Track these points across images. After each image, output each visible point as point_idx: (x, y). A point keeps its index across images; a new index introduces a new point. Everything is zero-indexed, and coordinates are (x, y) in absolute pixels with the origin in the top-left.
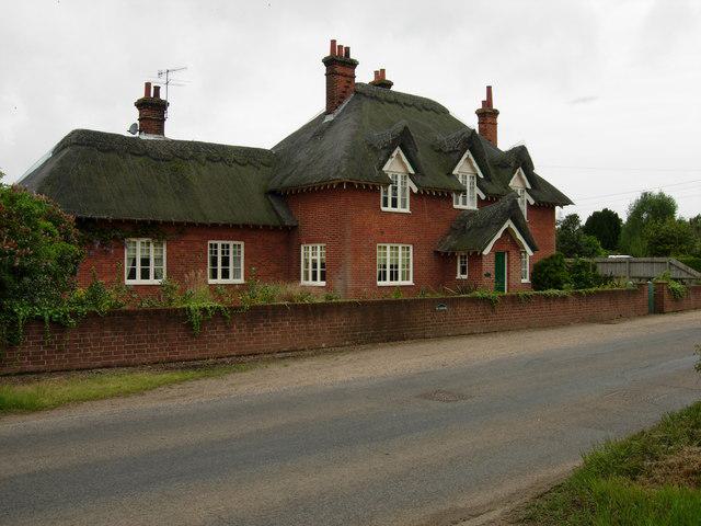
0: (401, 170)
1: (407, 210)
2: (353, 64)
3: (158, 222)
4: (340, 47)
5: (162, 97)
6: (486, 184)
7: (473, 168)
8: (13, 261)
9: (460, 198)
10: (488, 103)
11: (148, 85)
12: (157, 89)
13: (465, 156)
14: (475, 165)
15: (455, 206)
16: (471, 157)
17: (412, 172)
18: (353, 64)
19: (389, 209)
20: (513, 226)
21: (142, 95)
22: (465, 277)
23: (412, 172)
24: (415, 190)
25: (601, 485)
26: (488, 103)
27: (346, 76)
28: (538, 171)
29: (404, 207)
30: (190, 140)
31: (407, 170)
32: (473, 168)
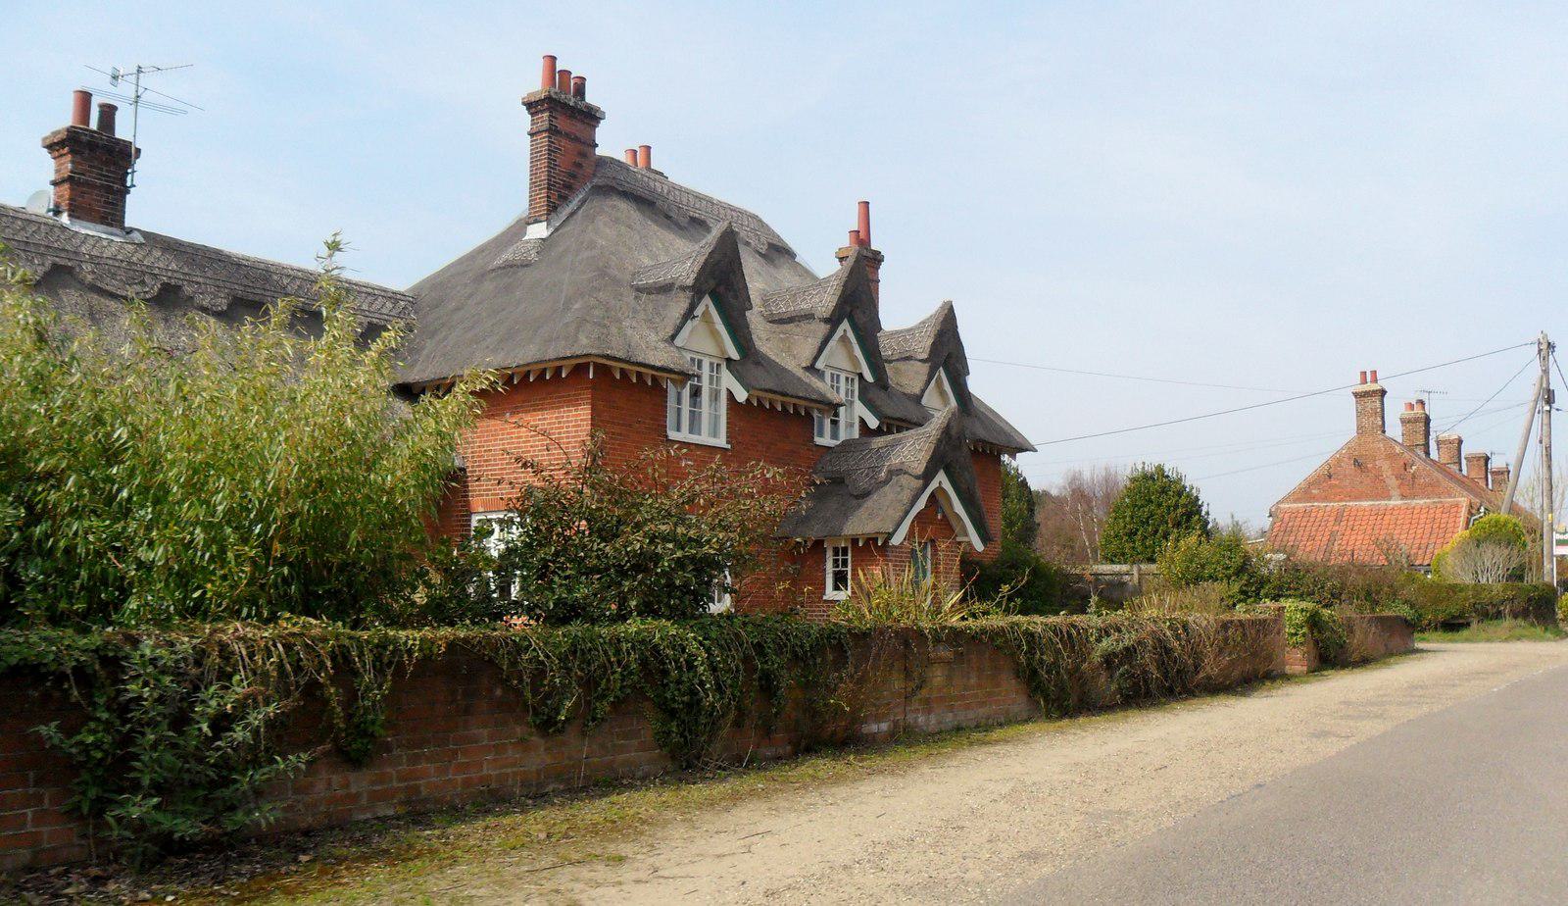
0: (711, 348)
1: (721, 441)
2: (592, 117)
3: (920, 634)
4: (565, 73)
5: (122, 131)
6: (873, 394)
7: (853, 359)
8: (119, 596)
9: (827, 423)
10: (862, 238)
11: (85, 99)
12: (108, 113)
13: (839, 333)
14: (858, 352)
15: (818, 440)
16: (851, 335)
17: (735, 355)
18: (592, 117)
19: (684, 435)
20: (947, 486)
21: (64, 118)
22: (842, 596)
23: (735, 355)
24: (741, 396)
25: (1282, 506)
26: (862, 238)
27: (577, 140)
28: (975, 385)
29: (715, 434)
30: (126, 210)
31: (723, 350)
32: (853, 359)
